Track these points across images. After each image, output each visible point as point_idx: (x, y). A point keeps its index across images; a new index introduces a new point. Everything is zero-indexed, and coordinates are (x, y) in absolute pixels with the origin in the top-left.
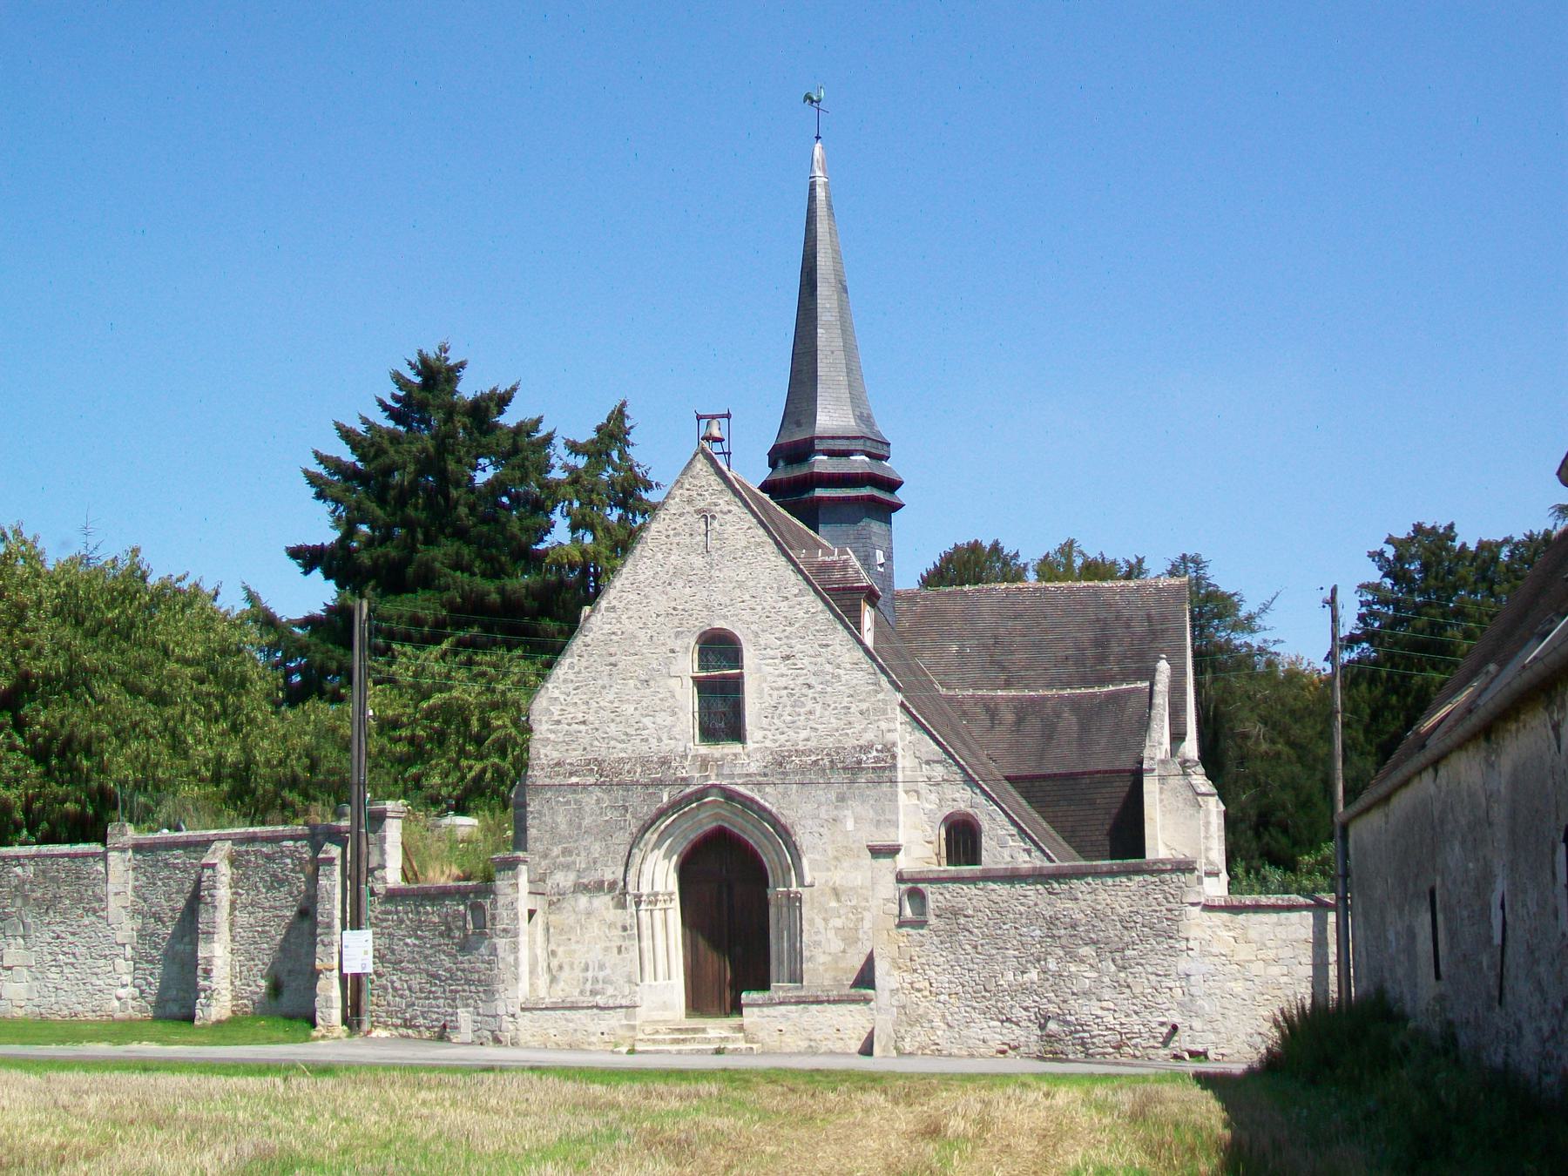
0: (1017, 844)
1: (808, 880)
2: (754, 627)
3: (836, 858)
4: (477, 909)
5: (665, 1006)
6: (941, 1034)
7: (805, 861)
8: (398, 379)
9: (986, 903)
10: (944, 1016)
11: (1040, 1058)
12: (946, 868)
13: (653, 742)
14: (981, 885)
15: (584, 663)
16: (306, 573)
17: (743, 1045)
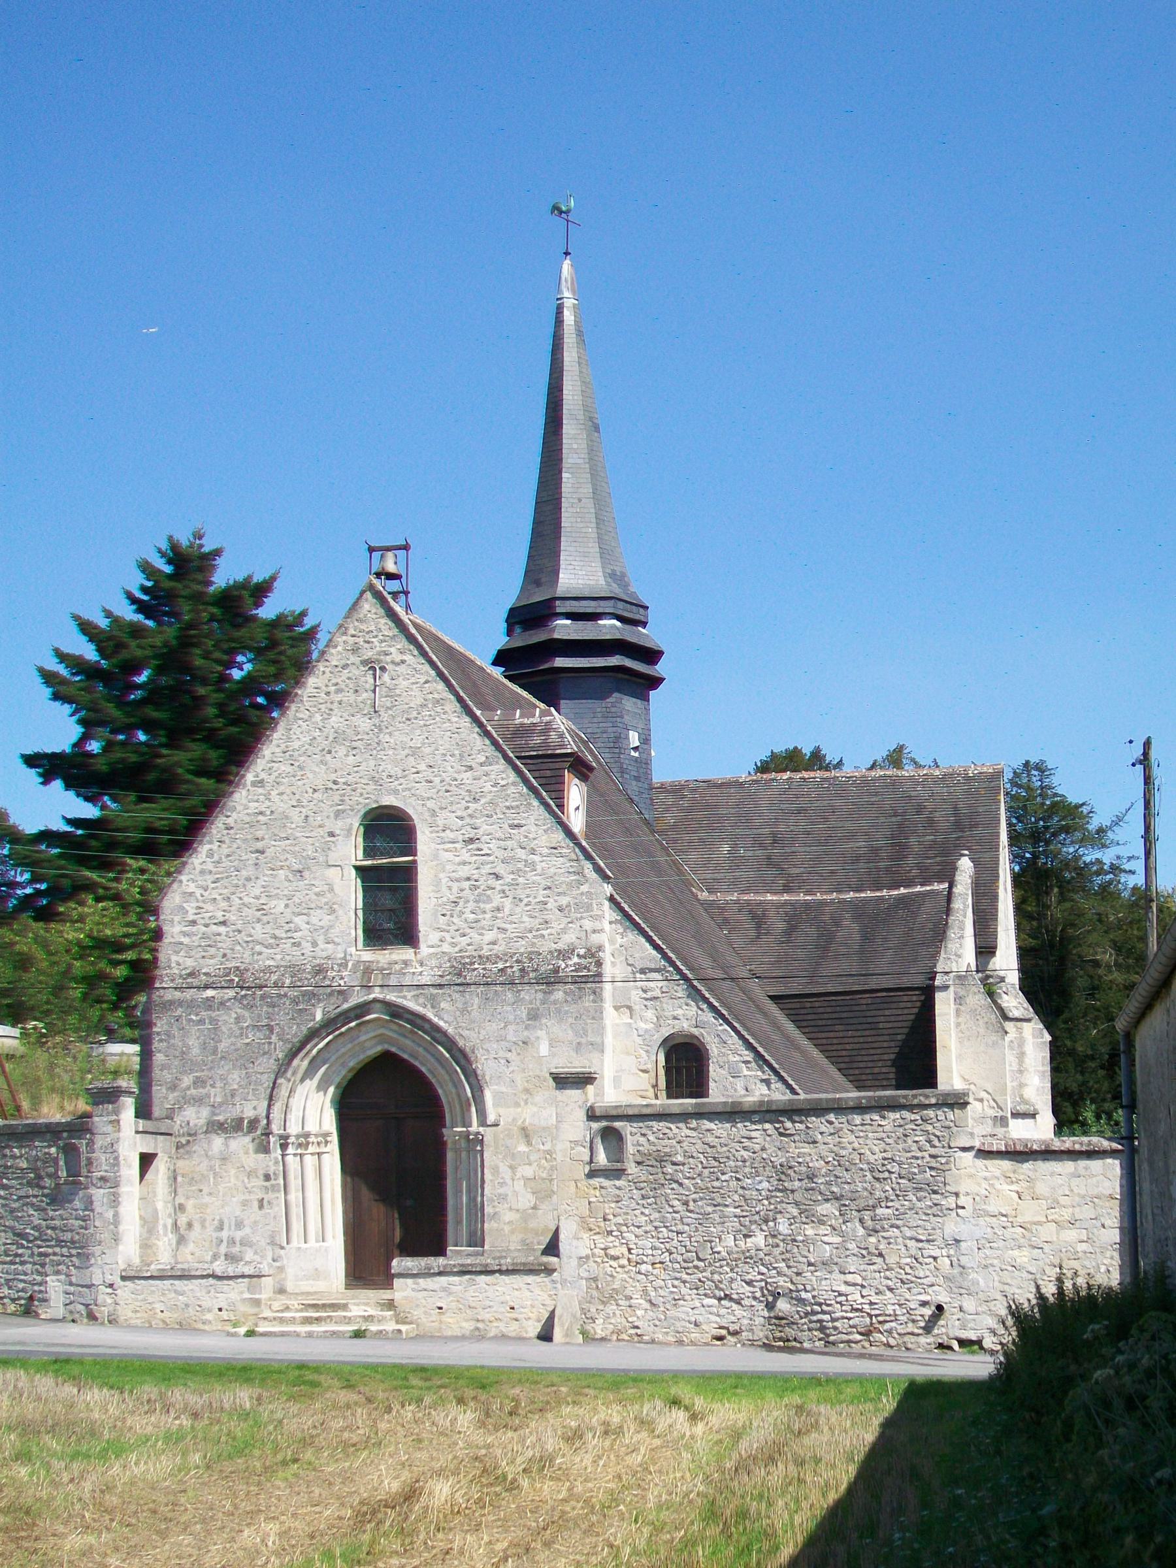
0: (754, 1073)
1: (491, 1118)
2: (430, 804)
3: (527, 1091)
4: (70, 1151)
5: (317, 1274)
6: (642, 1315)
7: (488, 1096)
8: (146, 568)
9: (699, 1146)
10: (645, 1291)
11: (768, 1347)
12: (663, 1102)
13: (307, 947)
14: (694, 1124)
15: (225, 850)
16: (45, 783)
17: (391, 1326)
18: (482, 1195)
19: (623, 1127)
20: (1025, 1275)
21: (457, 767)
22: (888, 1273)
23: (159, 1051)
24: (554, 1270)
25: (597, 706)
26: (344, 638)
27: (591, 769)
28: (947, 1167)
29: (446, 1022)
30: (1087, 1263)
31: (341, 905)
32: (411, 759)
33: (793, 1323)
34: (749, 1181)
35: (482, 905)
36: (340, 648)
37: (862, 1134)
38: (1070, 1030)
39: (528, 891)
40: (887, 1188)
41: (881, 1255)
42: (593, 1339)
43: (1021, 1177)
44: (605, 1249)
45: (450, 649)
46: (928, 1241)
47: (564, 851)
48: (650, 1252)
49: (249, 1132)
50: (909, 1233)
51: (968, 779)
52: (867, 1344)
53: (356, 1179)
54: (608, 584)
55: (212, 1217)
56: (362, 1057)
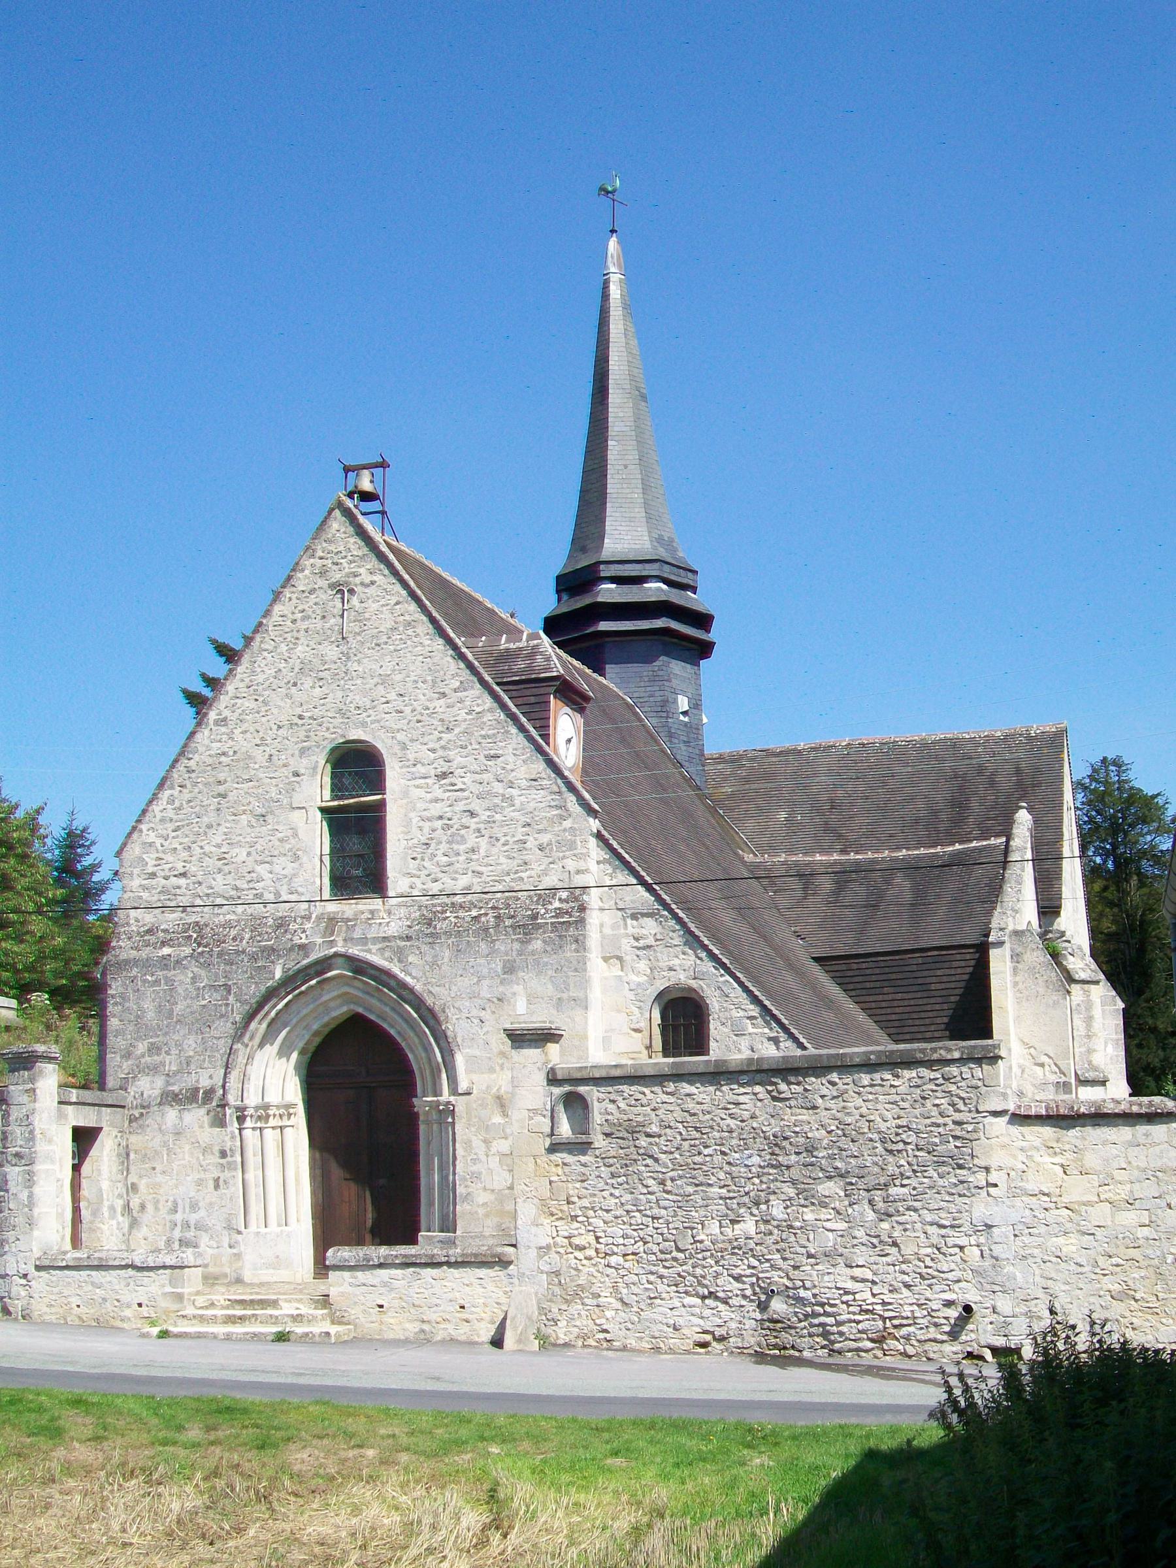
1: (463, 1086)
2: (400, 736)
7: (459, 1059)
9: (678, 1115)
11: (760, 1358)
14: (671, 1087)
15: (187, 795)
17: (327, 1326)
18: (454, 1174)
19: (589, 1092)
20: (1073, 1267)
21: (429, 694)
22: (904, 1267)
23: (114, 1016)
24: (511, 1263)
25: (644, 670)
26: (312, 561)
27: (587, 699)
28: (975, 1136)
29: (414, 978)
30: (1149, 1252)
31: (305, 851)
32: (380, 687)
33: (790, 1327)
34: (737, 1156)
35: (455, 847)
36: (307, 572)
37: (871, 1097)
38: (1151, 1009)
39: (505, 829)
40: (902, 1162)
41: (895, 1244)
42: (555, 1345)
43: (1067, 1147)
44: (569, 1238)
45: (445, 584)
46: (952, 1226)
47: (545, 782)
48: (621, 1241)
49: (204, 1103)
50: (929, 1218)
51: (1030, 738)
52: (879, 1353)
53: (326, 1155)
54: (655, 548)
55: (165, 1198)
56: (326, 1019)
